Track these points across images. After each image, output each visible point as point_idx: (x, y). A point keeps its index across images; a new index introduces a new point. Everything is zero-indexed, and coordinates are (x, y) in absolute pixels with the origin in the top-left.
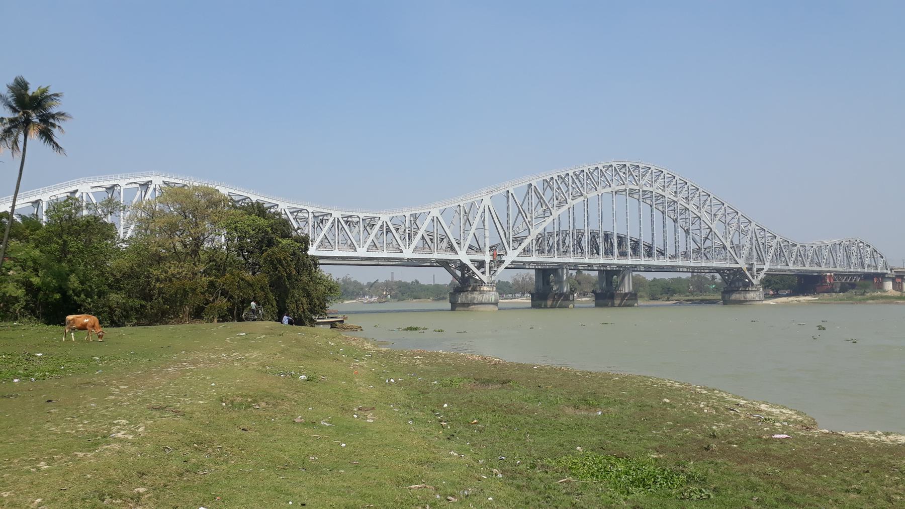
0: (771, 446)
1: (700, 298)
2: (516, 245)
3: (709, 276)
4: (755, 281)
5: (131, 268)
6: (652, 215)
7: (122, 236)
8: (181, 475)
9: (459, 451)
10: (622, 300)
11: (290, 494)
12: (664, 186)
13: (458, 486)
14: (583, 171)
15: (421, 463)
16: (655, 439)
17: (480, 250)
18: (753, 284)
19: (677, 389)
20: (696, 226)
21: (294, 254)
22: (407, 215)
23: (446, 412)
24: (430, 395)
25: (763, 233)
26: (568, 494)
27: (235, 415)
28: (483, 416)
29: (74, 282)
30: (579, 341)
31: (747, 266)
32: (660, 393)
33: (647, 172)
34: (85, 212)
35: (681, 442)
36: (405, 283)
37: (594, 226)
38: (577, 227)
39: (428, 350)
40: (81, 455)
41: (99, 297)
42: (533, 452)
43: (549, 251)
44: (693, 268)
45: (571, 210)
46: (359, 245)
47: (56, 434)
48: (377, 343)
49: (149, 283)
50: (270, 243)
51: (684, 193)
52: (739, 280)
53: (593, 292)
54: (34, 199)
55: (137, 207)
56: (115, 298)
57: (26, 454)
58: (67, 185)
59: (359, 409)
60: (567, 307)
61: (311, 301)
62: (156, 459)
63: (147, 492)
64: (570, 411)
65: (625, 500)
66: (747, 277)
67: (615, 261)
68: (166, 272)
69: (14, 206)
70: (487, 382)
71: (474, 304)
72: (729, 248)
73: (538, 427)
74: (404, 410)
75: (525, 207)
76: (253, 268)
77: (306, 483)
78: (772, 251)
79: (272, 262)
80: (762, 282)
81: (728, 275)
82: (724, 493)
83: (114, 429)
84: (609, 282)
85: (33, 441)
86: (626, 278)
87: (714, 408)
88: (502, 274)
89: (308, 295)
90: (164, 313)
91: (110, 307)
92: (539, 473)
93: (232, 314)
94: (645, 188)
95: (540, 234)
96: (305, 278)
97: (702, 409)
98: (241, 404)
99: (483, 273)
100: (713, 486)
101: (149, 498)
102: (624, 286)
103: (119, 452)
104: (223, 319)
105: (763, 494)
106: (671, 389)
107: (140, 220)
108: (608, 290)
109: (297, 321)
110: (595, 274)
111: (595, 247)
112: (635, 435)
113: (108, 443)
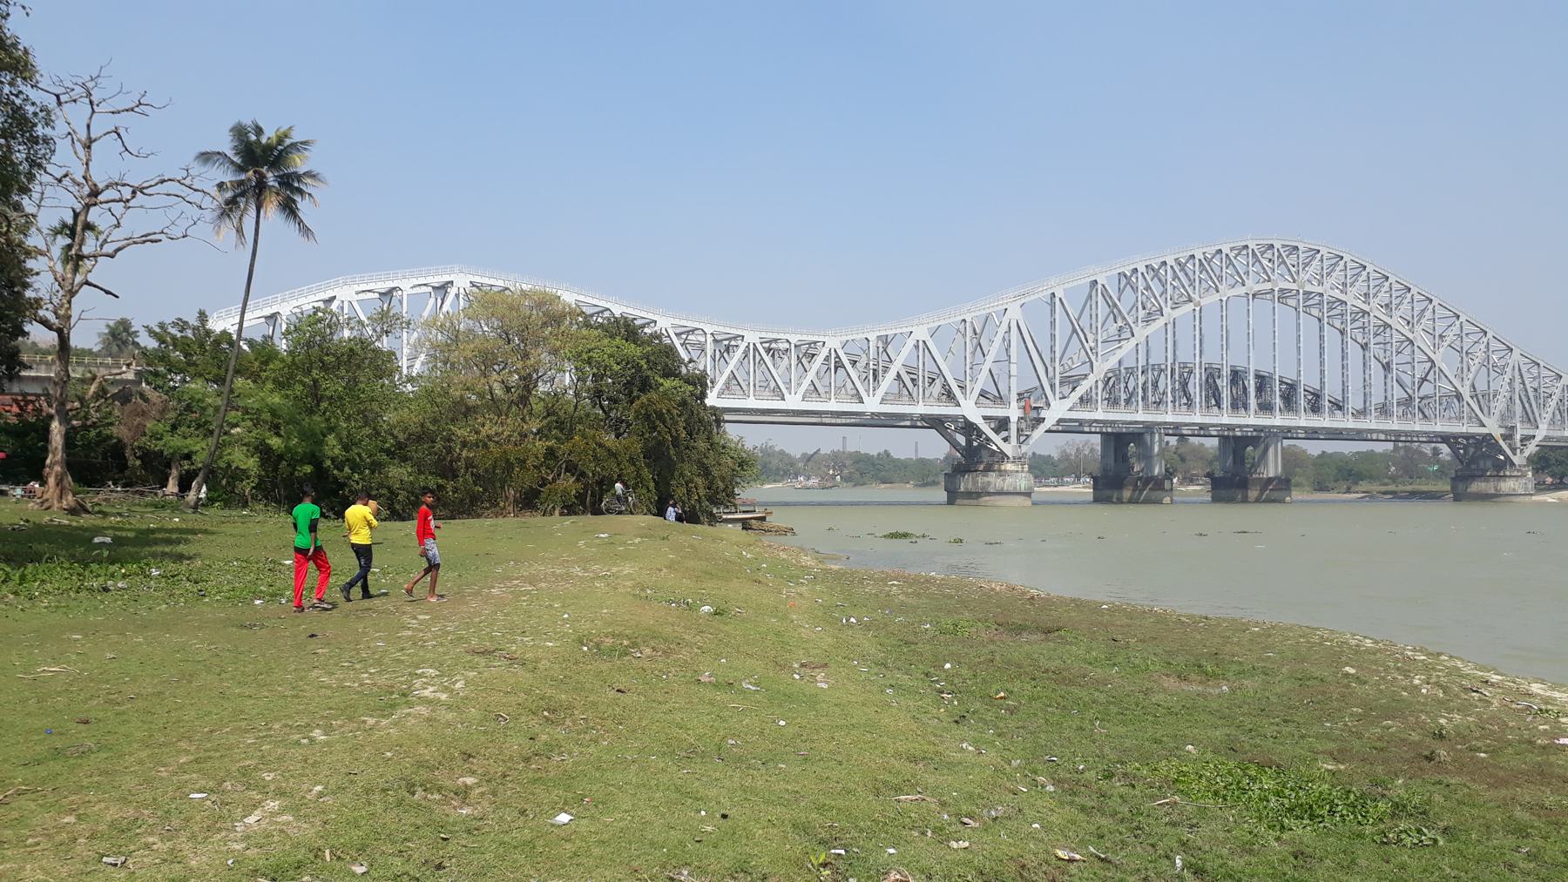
0: (1552, 758)
1: (1409, 488)
2: (1066, 390)
3: (1427, 449)
4: (1517, 460)
5: (422, 425)
6: (1321, 338)
7: (405, 371)
8: (527, 760)
9: (975, 742)
10: (1262, 491)
11: (701, 799)
12: (1344, 284)
13: (979, 801)
14: (1164, 263)
15: (913, 760)
16: (1328, 737)
17: (1000, 399)
18: (1512, 464)
19: (1368, 651)
20: (1405, 357)
21: (684, 403)
22: (872, 337)
23: (949, 677)
24: (920, 647)
25: (1535, 371)
26: (1174, 824)
27: (605, 667)
28: (1016, 686)
29: (332, 446)
30: (1182, 560)
31: (1502, 431)
32: (1336, 657)
33: (1313, 257)
34: (347, 333)
35: (1379, 744)
36: (866, 455)
37: (1212, 357)
38: (1180, 359)
39: (912, 572)
40: (371, 721)
41: (373, 472)
42: (1107, 750)
43: (1128, 401)
44: (1398, 434)
45: (1170, 327)
46: (789, 389)
47: (329, 687)
48: (821, 558)
49: (450, 450)
50: (645, 386)
51: (1383, 297)
52: (1484, 456)
53: (1208, 475)
54: (268, 311)
55: (430, 324)
56: (398, 473)
57: (290, 717)
58: (319, 290)
59: (803, 665)
60: (1159, 502)
61: (711, 483)
62: (485, 732)
63: (479, 785)
64: (1171, 683)
65: (1278, 839)
66: (1502, 452)
67: (1251, 419)
68: (477, 432)
69: (241, 323)
70: (1019, 629)
71: (989, 494)
72: (1467, 397)
73: (1114, 709)
74: (876, 670)
75: (1085, 322)
76: (617, 427)
77: (727, 783)
78: (1553, 403)
79: (647, 417)
80: (1530, 460)
81: (1465, 448)
82: (1463, 838)
83: (418, 683)
84: (1239, 458)
85: (296, 696)
86: (1271, 451)
87: (1441, 686)
88: (1041, 442)
89: (706, 472)
90: (475, 499)
91: (389, 488)
92: (1118, 786)
93: (583, 503)
94: (1308, 288)
95: (1110, 371)
96: (702, 445)
97: (1416, 687)
98: (612, 649)
99: (1005, 440)
100: (1441, 825)
101: (483, 794)
102: (1266, 465)
103: (429, 720)
104: (569, 510)
105: (1540, 842)
106: (1357, 650)
107: (434, 347)
108: (1236, 473)
109: (689, 517)
110: (1212, 443)
111: (1213, 395)
112: (1291, 728)
113: (410, 705)
